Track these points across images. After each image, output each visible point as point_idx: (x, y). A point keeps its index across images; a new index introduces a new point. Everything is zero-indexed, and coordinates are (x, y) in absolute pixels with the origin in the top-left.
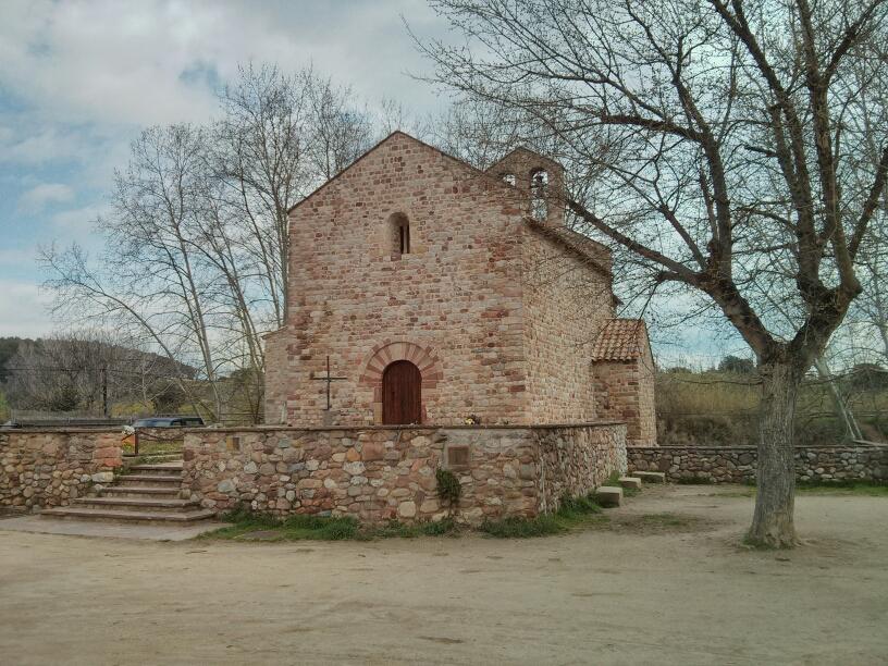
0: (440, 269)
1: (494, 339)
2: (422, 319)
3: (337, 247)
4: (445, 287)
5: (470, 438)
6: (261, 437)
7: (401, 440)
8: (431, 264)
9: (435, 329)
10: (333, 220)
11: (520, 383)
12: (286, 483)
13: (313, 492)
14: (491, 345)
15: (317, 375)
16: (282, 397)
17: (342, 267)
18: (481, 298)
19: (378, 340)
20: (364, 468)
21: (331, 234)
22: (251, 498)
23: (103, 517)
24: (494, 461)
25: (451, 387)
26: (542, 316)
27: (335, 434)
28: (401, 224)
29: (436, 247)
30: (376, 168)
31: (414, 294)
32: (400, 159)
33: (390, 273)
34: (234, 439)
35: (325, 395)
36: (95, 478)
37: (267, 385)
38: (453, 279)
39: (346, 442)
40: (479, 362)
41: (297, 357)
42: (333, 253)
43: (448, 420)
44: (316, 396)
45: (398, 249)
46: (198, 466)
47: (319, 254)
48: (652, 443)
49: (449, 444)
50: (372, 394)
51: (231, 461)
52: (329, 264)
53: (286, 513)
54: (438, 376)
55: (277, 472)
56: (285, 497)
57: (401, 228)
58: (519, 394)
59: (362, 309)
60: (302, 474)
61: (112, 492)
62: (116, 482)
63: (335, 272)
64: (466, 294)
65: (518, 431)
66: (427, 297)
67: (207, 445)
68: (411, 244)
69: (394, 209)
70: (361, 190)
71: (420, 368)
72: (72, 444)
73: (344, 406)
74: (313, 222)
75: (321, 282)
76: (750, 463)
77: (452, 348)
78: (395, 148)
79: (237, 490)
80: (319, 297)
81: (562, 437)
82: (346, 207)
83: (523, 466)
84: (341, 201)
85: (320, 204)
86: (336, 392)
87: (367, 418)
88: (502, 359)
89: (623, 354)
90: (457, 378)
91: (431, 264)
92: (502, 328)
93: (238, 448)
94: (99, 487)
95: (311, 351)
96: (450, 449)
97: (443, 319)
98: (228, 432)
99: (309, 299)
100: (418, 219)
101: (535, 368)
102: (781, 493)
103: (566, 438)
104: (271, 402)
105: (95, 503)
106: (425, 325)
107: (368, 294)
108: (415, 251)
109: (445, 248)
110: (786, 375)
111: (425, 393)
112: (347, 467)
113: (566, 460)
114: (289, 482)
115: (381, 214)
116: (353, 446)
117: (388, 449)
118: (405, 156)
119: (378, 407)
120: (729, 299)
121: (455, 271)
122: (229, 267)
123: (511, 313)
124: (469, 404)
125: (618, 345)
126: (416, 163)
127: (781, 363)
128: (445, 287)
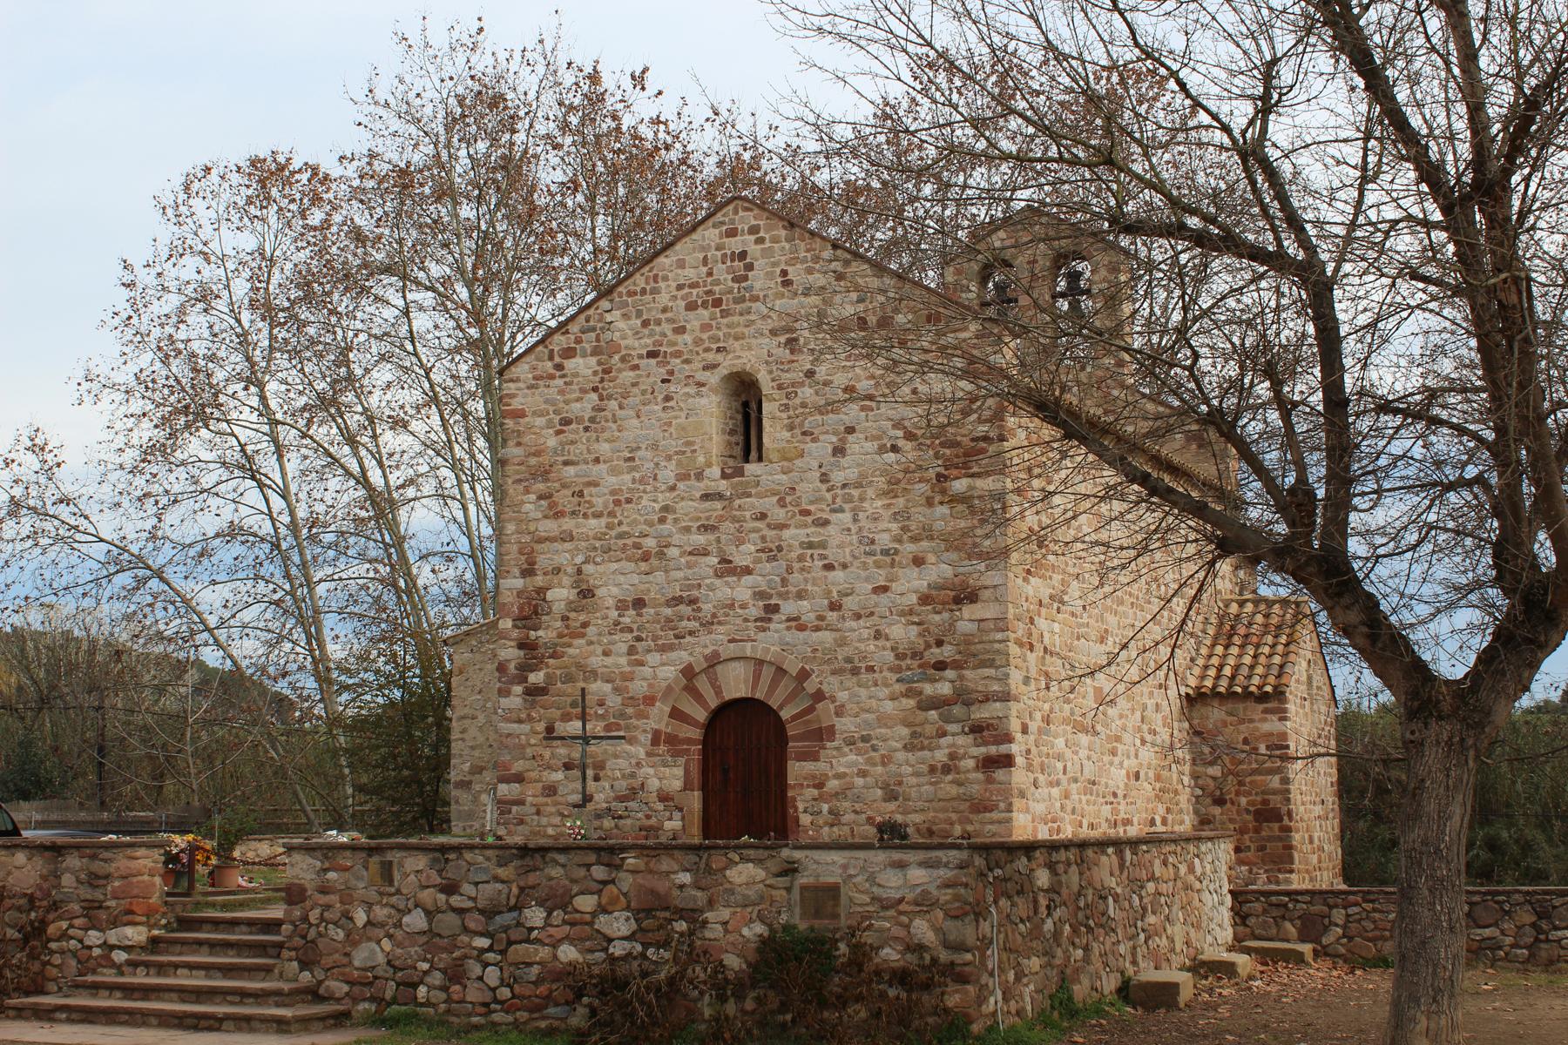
0: (828, 496)
1: (947, 652)
2: (788, 608)
3: (604, 448)
4: (839, 536)
5: (845, 867)
6: (435, 860)
7: (709, 870)
8: (809, 487)
9: (817, 629)
10: (595, 389)
11: (1003, 749)
12: (483, 951)
13: (535, 970)
14: (941, 666)
15: (562, 728)
16: (488, 776)
17: (613, 493)
18: (918, 561)
19: (692, 653)
20: (634, 926)
21: (592, 420)
22: (416, 979)
23: (130, 1012)
24: (892, 913)
25: (853, 757)
26: (1058, 599)
27: (578, 857)
28: (743, 398)
29: (820, 450)
30: (690, 274)
31: (772, 552)
32: (743, 255)
33: (718, 505)
34: (383, 863)
35: (576, 773)
36: (113, 936)
37: (456, 747)
38: (855, 520)
39: (599, 872)
40: (912, 703)
41: (518, 689)
42: (597, 460)
43: (846, 829)
44: (559, 776)
45: (738, 451)
46: (314, 916)
47: (566, 463)
48: (1328, 878)
49: (803, 879)
50: (679, 772)
51: (377, 908)
52: (589, 484)
53: (483, 1010)
54: (822, 734)
55: (466, 930)
56: (481, 978)
57: (746, 405)
58: (1000, 774)
59: (658, 585)
60: (515, 934)
61: (147, 965)
62: (154, 944)
63: (599, 503)
64: (885, 552)
65: (939, 853)
66: (801, 558)
67: (332, 875)
68: (765, 440)
69: (727, 364)
70: (658, 322)
71: (785, 714)
72: (67, 870)
73: (621, 799)
74: (552, 393)
75: (568, 524)
76: (1496, 924)
77: (855, 672)
78: (732, 233)
79: (389, 963)
80: (562, 556)
81: (1051, 866)
82: (623, 359)
83: (949, 924)
84: (613, 348)
85: (569, 353)
86: (600, 766)
87: (668, 825)
88: (963, 697)
89: (1256, 680)
90: (865, 739)
91: (809, 487)
92: (965, 626)
93: (391, 882)
94: (120, 956)
95: (547, 676)
96: (804, 888)
97: (834, 606)
98: (371, 851)
99: (543, 562)
100: (780, 387)
101: (1038, 715)
102: (1434, 973)
103: (1061, 868)
104: (464, 785)
105: (112, 988)
106: (796, 623)
107: (673, 552)
108: (774, 456)
109: (839, 451)
110: (1449, 743)
111: (796, 770)
112: (602, 922)
113: (1058, 913)
114: (490, 949)
115: (701, 376)
116: (613, 882)
117: (682, 887)
118: (754, 249)
119: (695, 800)
120: (1340, 595)
121: (862, 499)
122: (375, 477)
123: (986, 594)
124: (891, 796)
125: (1247, 660)
126: (774, 264)
127: (1440, 718)
128: (839, 536)
